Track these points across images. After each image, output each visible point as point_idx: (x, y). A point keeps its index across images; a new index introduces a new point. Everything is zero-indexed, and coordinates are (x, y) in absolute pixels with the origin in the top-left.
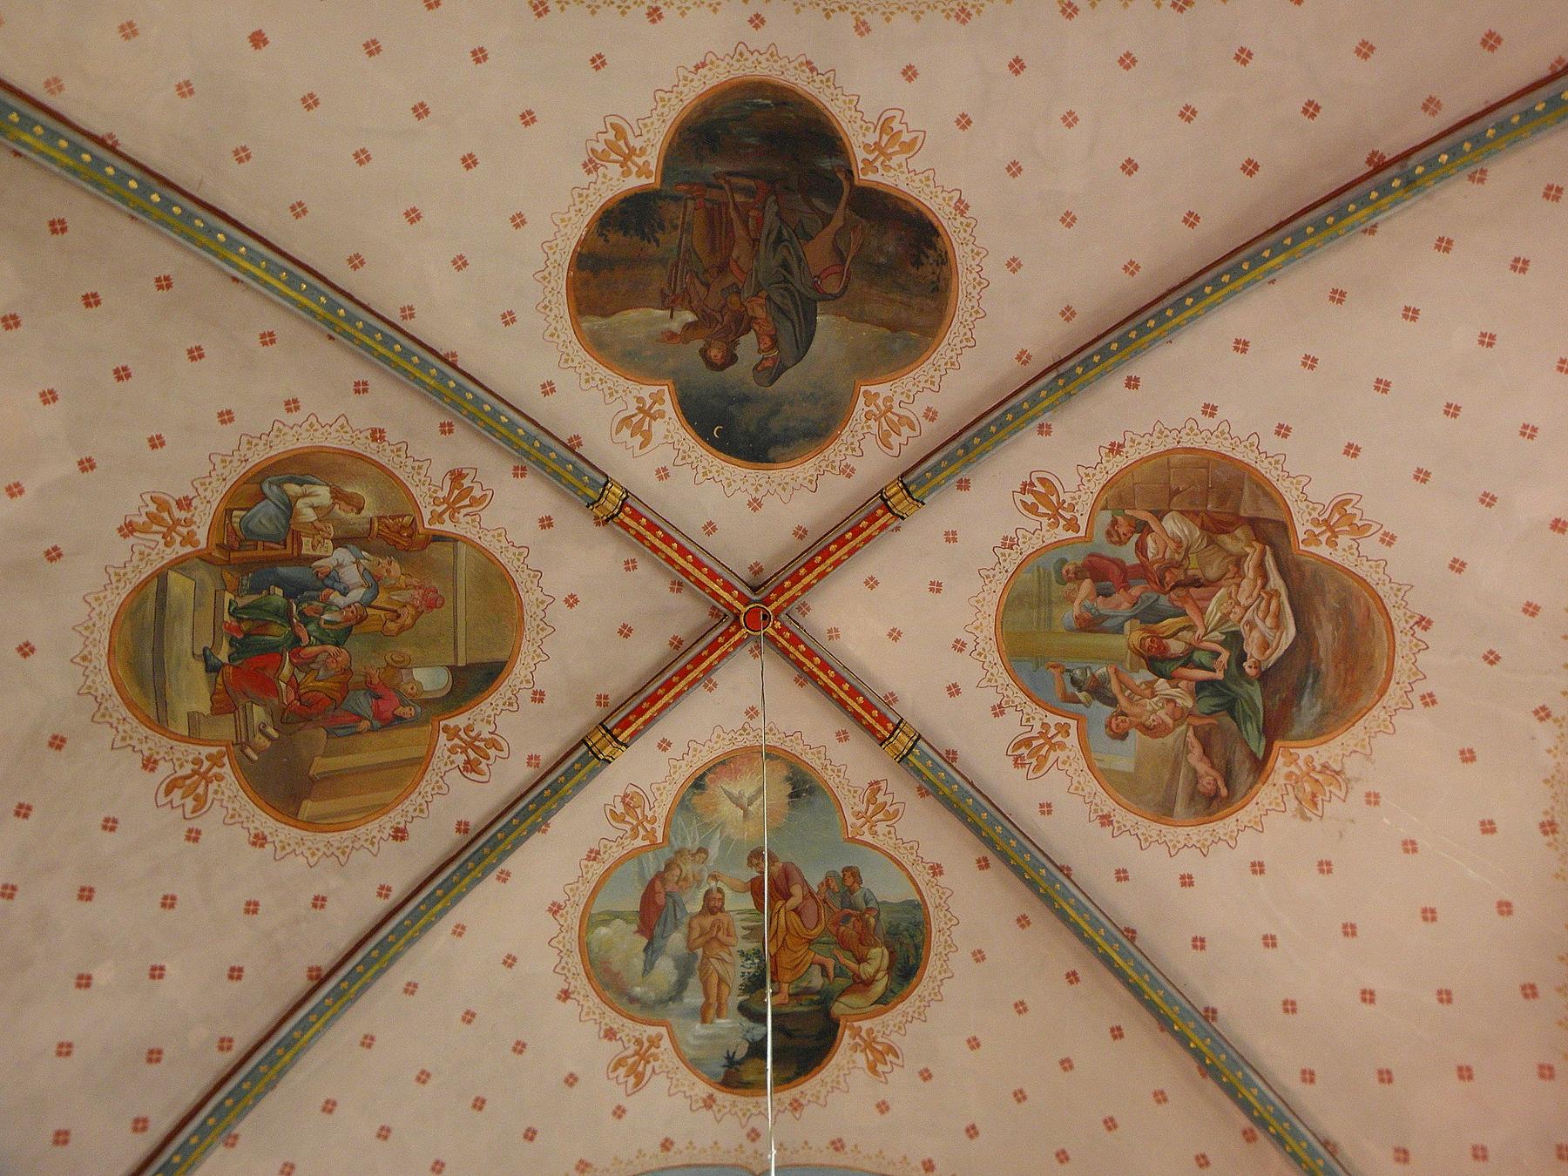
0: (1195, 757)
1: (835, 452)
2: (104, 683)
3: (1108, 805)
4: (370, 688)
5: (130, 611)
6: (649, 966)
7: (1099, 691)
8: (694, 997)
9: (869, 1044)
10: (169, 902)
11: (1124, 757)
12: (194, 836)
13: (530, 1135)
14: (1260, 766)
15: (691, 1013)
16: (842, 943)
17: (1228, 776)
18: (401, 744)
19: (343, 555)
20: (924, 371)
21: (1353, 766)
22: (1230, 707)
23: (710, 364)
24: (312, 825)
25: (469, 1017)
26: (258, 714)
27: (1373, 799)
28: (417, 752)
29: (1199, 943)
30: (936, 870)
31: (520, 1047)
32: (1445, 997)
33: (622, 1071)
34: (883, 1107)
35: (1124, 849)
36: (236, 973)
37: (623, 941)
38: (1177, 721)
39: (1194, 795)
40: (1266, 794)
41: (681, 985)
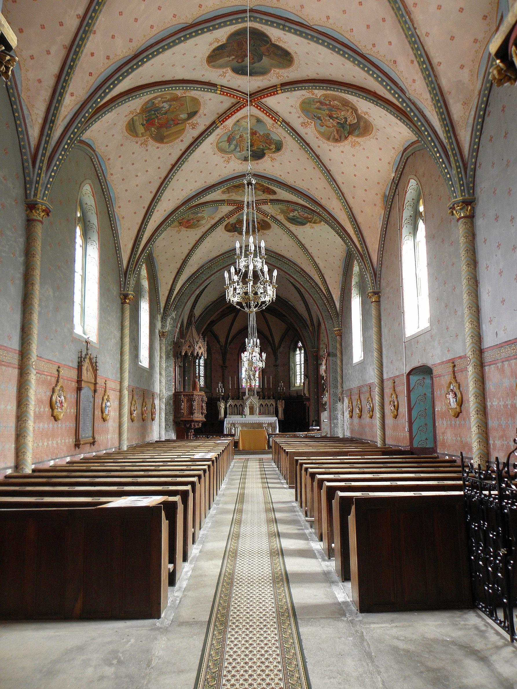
0: (335, 133)
1: (268, 76)
2: (126, 134)
3: (318, 136)
4: (172, 120)
5: (129, 123)
6: (229, 147)
7: (319, 118)
8: (238, 149)
9: (271, 157)
10: (146, 161)
11: (322, 130)
12: (147, 150)
14: (346, 138)
15: (238, 152)
16: (267, 143)
17: (340, 137)
18: (180, 127)
19: (164, 104)
20: (287, 70)
21: (362, 143)
22: (343, 127)
23: (238, 62)
24: (166, 143)
26: (153, 129)
27: (364, 149)
28: (183, 128)
29: (330, 160)
30: (285, 138)
34: (273, 166)
35: (320, 143)
36: (159, 168)
37: (225, 145)
38: (333, 127)
39: (334, 138)
40: (346, 142)
41: (236, 148)
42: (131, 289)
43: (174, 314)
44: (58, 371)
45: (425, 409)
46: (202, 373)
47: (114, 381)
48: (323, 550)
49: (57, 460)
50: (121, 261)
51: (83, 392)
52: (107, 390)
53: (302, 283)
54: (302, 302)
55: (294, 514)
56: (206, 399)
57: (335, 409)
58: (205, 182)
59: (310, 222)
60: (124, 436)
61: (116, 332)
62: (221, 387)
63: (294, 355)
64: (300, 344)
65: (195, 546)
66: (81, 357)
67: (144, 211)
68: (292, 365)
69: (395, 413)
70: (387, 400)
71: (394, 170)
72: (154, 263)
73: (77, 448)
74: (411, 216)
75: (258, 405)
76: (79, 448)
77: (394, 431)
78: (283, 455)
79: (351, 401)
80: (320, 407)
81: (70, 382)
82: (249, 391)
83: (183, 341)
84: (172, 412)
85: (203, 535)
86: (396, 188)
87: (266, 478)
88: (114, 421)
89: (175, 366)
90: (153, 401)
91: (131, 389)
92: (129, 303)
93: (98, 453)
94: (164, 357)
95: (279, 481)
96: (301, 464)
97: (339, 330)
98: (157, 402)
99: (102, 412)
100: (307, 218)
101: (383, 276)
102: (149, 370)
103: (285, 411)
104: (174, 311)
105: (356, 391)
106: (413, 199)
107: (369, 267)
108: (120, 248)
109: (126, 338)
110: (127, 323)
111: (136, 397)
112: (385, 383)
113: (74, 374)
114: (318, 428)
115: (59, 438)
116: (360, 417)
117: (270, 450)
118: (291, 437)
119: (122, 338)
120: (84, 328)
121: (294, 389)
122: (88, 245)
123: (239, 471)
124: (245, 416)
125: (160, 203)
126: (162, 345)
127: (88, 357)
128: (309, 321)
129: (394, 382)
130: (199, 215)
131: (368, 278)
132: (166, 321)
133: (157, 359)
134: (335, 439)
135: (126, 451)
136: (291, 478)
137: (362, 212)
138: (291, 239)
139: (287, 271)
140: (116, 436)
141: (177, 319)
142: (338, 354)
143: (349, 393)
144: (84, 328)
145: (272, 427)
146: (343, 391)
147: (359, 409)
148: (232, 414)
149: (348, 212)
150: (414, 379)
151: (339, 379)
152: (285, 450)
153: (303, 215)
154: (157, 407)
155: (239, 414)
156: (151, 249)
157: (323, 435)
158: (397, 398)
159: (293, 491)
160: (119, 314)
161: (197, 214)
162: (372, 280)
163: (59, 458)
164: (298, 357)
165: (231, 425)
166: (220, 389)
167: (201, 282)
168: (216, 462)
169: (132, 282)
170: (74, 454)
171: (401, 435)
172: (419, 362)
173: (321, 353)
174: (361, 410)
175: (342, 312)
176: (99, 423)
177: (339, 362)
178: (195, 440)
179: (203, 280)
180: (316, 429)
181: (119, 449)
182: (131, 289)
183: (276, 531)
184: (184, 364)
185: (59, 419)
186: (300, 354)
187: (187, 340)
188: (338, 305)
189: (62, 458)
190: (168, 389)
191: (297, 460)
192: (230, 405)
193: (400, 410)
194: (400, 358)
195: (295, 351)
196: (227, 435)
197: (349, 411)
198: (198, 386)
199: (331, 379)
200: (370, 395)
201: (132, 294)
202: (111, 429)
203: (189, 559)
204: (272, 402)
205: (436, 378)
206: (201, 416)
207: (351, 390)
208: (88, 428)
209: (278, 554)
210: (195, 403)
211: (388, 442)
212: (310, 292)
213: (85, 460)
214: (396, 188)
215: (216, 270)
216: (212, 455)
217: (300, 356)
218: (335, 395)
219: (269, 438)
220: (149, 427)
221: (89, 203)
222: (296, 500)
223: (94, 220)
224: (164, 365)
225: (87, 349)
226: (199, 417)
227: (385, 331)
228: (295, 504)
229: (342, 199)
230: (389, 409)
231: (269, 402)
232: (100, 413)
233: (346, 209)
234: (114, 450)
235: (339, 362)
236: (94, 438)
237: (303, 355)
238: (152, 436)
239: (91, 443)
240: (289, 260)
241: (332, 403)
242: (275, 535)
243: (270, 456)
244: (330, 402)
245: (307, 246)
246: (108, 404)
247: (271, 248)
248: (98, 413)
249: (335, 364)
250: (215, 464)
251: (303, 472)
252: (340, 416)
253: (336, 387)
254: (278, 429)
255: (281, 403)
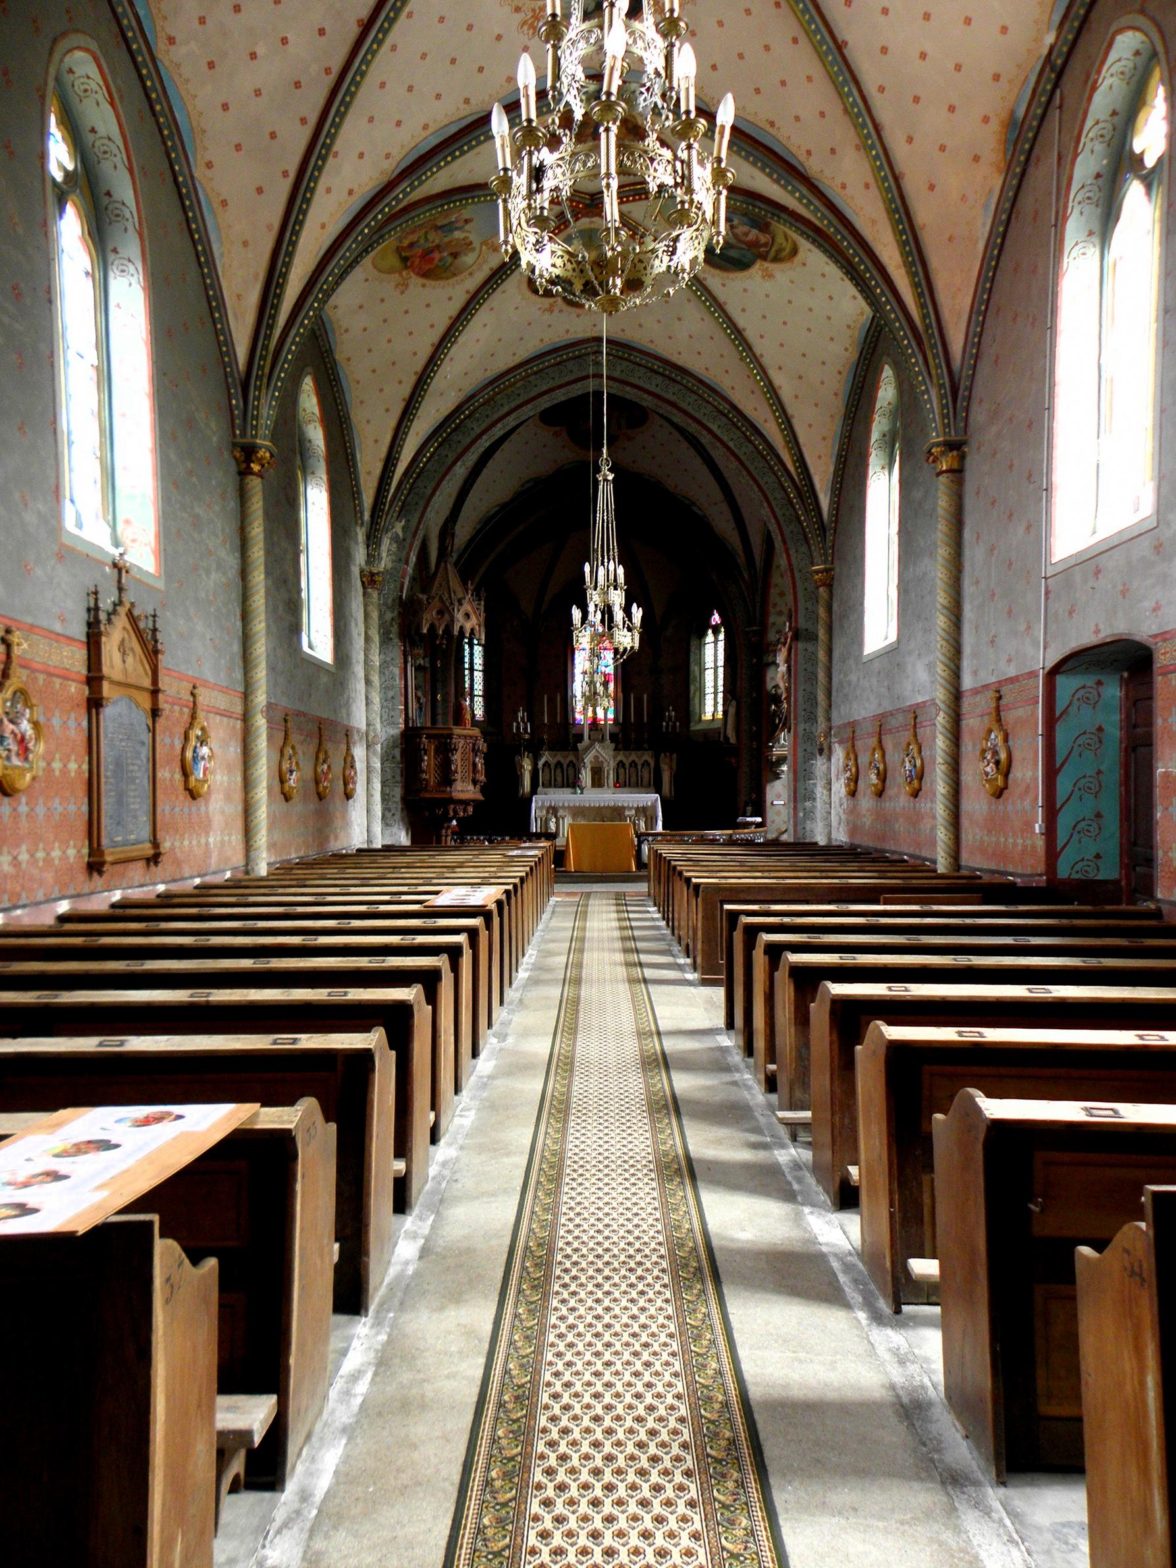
13: (481, 70)
25: (442, 19)
31: (470, 27)
32: (958, 68)
33: (525, 28)
42: (264, 431)
43: (398, 528)
44: (193, 694)
45: (1099, 772)
46: (479, 687)
47: (224, 690)
48: (860, 1255)
49: (19, 912)
50: (229, 343)
51: (108, 712)
52: (201, 715)
53: (731, 444)
54: (724, 507)
55: (726, 1077)
56: (482, 745)
57: (809, 775)
58: (467, 101)
59: (764, 257)
60: (259, 836)
61: (223, 553)
62: (523, 718)
63: (701, 646)
64: (716, 618)
65: (409, 1222)
66: (97, 608)
67: (286, 185)
68: (694, 668)
69: (1000, 782)
70: (969, 748)
71: (1057, 18)
72: (337, 379)
73: (95, 875)
74: (1098, 176)
75: (612, 764)
76: (100, 873)
77: (989, 832)
78: (682, 893)
79: (852, 753)
80: (766, 770)
81: (58, 681)
82: (591, 730)
83: (424, 597)
84: (398, 778)
85: (444, 1164)
86: (1056, 85)
87: (634, 939)
88: (228, 798)
89: (406, 662)
90: (348, 749)
91: (279, 716)
92: (259, 475)
93: (175, 887)
94: (376, 638)
95: (669, 959)
96: (752, 932)
97: (827, 571)
98: (359, 752)
99: (186, 774)
100: (754, 244)
101: (978, 391)
102: (333, 670)
103: (676, 779)
104: (398, 518)
105: (871, 728)
106: (1114, 113)
107: (938, 366)
108: (222, 306)
109: (256, 573)
110: (257, 530)
111: (295, 738)
112: (967, 704)
113: (75, 659)
114: (759, 820)
115: (24, 848)
116: (880, 793)
117: (643, 873)
118: (695, 843)
119: (244, 573)
120: (114, 528)
121: (699, 727)
122: (111, 275)
123: (565, 929)
124: (582, 790)
125: (331, 161)
126: (370, 608)
127: (122, 611)
128: (743, 559)
129: (1000, 698)
130: (457, 234)
131: (933, 400)
132: (379, 545)
133: (358, 643)
134: (804, 849)
135: (262, 879)
136: (709, 956)
137: (932, 187)
138: (708, 318)
139: (693, 413)
140: (237, 838)
141: (408, 541)
142: (822, 634)
143: (847, 734)
144: (114, 528)
145: (646, 816)
146: (830, 729)
147: (878, 774)
148: (550, 786)
149: (888, 190)
150: (1066, 685)
151: (821, 697)
152: (688, 880)
153: (746, 234)
154: (360, 765)
155: (568, 786)
156: (315, 316)
157: (771, 836)
158: (920, 751)
159: (719, 993)
160: (232, 504)
161: (451, 231)
162: (943, 407)
163: (24, 906)
164: (709, 650)
165: (548, 812)
166: (521, 723)
167: (468, 440)
168: (509, 904)
169: (267, 411)
170: (86, 890)
171: (1015, 845)
172: (1097, 632)
173: (772, 636)
174: (883, 777)
175: (836, 522)
176: (172, 805)
177: (821, 655)
178: (457, 848)
179: (473, 435)
180: (752, 823)
181: (247, 872)
182: (264, 431)
183: (680, 1151)
184: (433, 665)
185: (200, 796)
186: (716, 642)
187: (433, 594)
188: (825, 501)
189: (38, 904)
190: (388, 721)
191: (734, 915)
192: (546, 764)
193: (1017, 773)
194: (1023, 627)
195: (703, 635)
196: (538, 836)
197: (848, 779)
198: (468, 717)
199: (800, 700)
200: (915, 735)
201: (267, 449)
202: (217, 820)
203: (376, 1296)
204: (647, 757)
205: (1164, 674)
206: (471, 787)
207: (853, 725)
208: (135, 817)
209: (678, 1172)
210: (457, 757)
211: (966, 859)
212: (752, 468)
213: (122, 912)
214: (1056, 85)
215: (506, 409)
216: (486, 896)
217: (716, 647)
218: (810, 737)
219: (640, 843)
220: (338, 814)
221: (102, 130)
222: (730, 1025)
223: (124, 190)
224: (376, 660)
225: (120, 589)
226: (465, 789)
227: (974, 554)
228: (726, 1041)
229: (872, 147)
230: (975, 772)
231: (640, 758)
232: (178, 776)
233: (885, 179)
234: (228, 875)
235: (821, 655)
236: (155, 844)
237: (721, 645)
238: (348, 836)
239: (148, 860)
240: (701, 382)
241: (800, 760)
242: (666, 1106)
243: (643, 887)
244: (795, 755)
245: (750, 335)
246: (205, 751)
247: (652, 346)
248: (169, 774)
249: (812, 660)
250: (506, 908)
251: (760, 959)
252: (820, 791)
253: (812, 718)
254: (660, 823)
255: (667, 760)
